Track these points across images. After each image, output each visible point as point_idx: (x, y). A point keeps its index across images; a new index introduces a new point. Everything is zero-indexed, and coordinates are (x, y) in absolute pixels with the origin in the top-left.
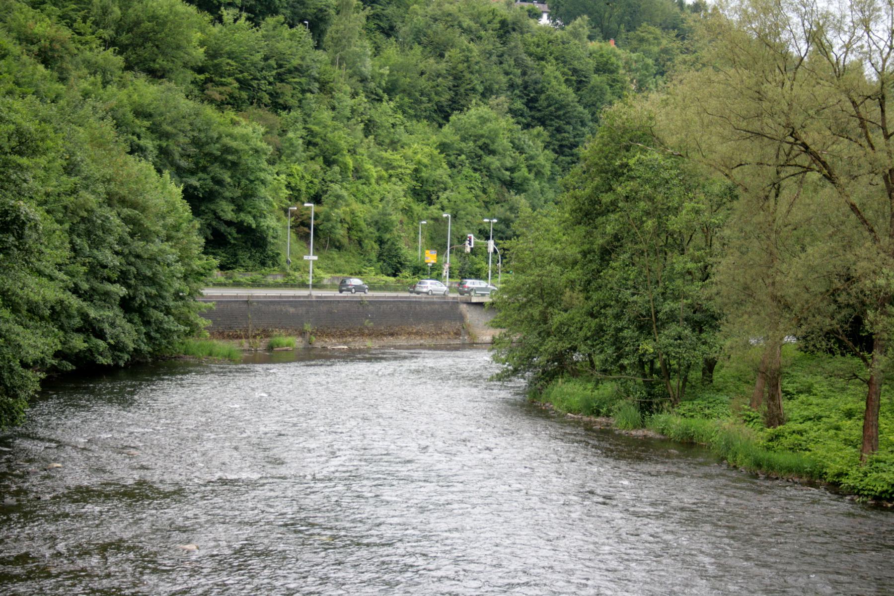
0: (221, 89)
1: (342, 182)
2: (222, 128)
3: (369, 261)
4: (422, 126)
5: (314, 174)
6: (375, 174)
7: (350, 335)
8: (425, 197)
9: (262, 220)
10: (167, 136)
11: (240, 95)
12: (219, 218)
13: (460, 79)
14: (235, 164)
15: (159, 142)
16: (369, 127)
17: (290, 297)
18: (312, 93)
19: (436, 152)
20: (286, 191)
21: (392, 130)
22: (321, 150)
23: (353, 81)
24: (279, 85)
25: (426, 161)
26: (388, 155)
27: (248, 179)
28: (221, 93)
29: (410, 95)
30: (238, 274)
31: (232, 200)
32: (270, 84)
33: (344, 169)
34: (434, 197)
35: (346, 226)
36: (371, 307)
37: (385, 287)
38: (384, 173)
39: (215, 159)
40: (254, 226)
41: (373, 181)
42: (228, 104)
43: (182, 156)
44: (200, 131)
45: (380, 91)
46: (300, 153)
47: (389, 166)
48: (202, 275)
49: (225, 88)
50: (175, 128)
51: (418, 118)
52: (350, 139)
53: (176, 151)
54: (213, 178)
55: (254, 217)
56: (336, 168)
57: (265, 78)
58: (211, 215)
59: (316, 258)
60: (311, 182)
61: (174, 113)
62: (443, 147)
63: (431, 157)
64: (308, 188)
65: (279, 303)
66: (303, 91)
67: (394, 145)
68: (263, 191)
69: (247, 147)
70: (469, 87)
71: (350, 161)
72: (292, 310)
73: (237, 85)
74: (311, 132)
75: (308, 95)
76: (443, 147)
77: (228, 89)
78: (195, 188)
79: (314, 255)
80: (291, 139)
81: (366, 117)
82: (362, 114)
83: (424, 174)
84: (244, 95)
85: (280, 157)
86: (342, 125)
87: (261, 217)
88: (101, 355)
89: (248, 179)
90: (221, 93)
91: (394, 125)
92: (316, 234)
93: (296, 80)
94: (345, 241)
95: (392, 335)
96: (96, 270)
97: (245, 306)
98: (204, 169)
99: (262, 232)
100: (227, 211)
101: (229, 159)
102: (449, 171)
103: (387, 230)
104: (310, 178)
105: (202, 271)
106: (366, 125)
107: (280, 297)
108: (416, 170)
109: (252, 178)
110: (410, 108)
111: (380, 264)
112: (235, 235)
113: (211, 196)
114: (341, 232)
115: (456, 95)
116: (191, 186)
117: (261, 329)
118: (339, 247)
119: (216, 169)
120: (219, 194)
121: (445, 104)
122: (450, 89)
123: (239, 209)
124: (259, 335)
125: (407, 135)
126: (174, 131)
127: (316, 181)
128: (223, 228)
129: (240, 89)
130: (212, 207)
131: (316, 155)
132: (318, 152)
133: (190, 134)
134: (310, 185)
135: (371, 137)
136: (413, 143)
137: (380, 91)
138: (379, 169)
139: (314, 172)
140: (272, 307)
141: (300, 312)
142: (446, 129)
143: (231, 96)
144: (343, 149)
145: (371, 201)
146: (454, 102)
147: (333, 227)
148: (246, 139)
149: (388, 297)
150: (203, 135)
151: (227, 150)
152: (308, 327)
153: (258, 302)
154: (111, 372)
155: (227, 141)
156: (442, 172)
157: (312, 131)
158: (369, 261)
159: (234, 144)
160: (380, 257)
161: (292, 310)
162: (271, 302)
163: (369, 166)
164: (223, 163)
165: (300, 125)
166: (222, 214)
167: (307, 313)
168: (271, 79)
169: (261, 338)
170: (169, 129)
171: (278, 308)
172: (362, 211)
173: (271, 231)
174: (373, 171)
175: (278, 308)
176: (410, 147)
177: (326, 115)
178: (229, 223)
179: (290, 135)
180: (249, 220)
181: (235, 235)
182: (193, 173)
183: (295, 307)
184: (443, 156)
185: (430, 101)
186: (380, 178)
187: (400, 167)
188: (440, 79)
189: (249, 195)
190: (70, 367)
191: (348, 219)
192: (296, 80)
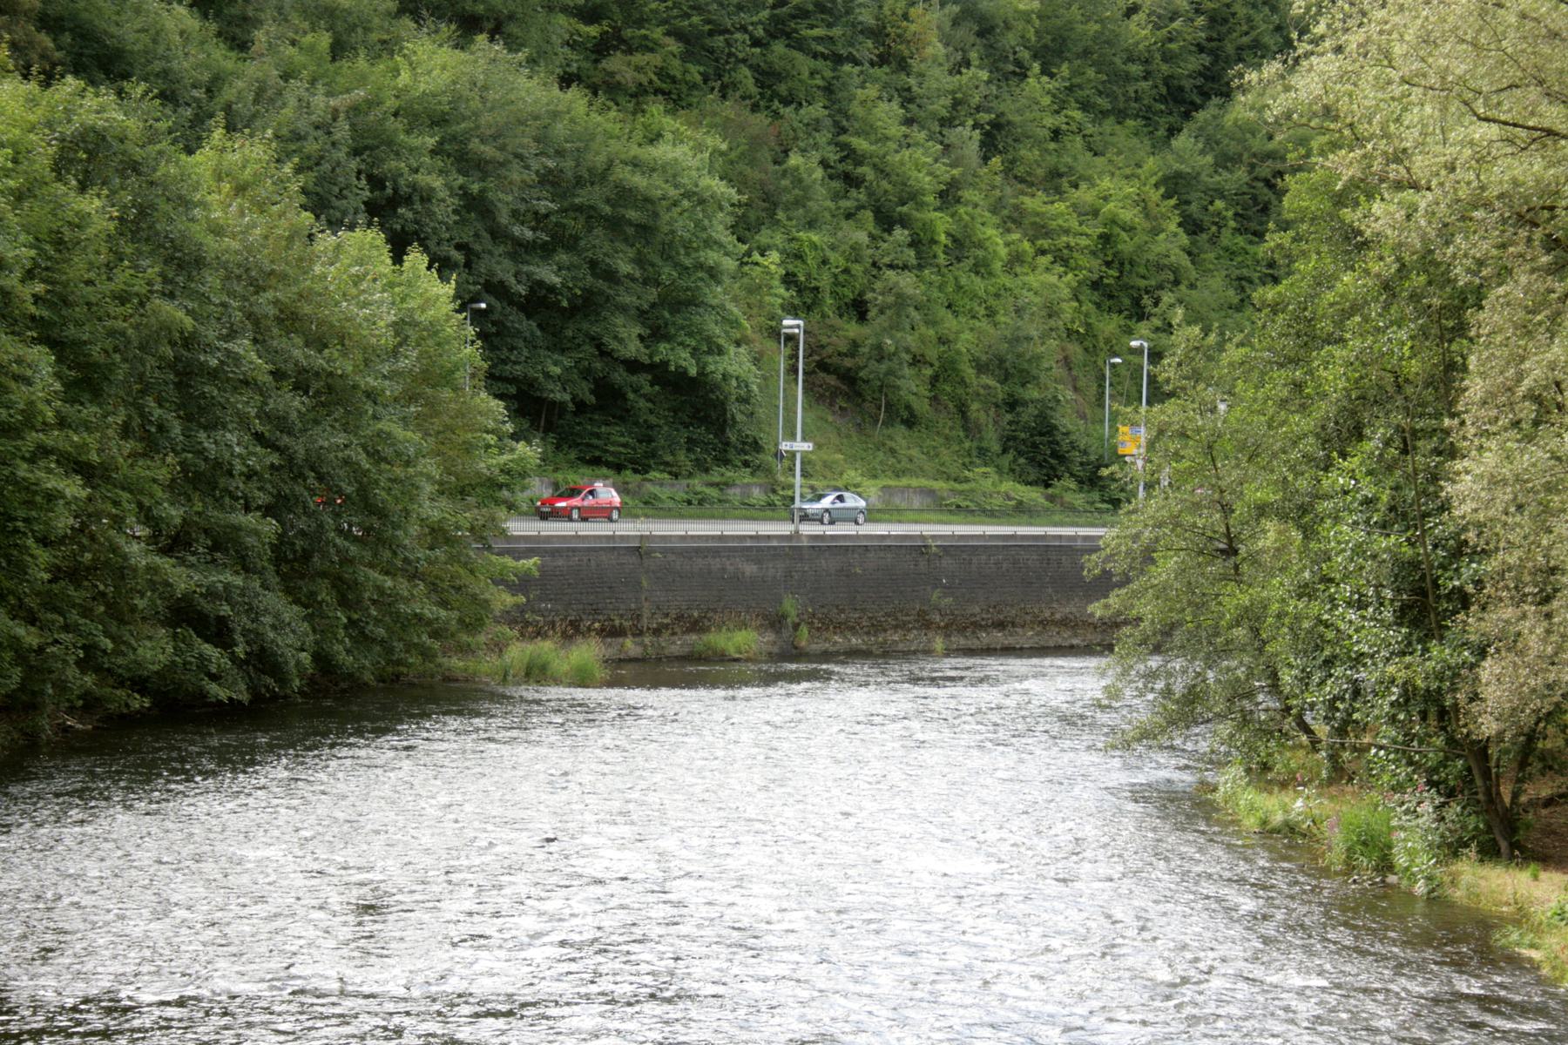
0: (638, 59)
1: (920, 267)
2: (615, 147)
3: (982, 452)
4: (1123, 136)
5: (855, 254)
6: (1003, 252)
7: (896, 627)
8: (1127, 302)
9: (710, 359)
10: (481, 167)
11: (686, 71)
12: (604, 353)
13: (1226, 21)
14: (645, 231)
15: (461, 180)
16: (994, 137)
17: (744, 537)
18: (857, 63)
19: (1155, 196)
20: (782, 291)
21: (1052, 145)
22: (870, 194)
23: (960, 33)
24: (779, 47)
25: (1128, 215)
26: (1034, 202)
27: (677, 265)
28: (638, 69)
29: (1098, 66)
30: (658, 484)
31: (642, 315)
32: (756, 43)
33: (920, 242)
34: (1147, 301)
35: (928, 372)
36: (947, 562)
37: (1021, 511)
38: (1026, 245)
39: (589, 213)
40: (693, 372)
41: (997, 266)
42: (657, 91)
43: (515, 214)
44: (560, 153)
45: (1025, 55)
46: (821, 198)
47: (1040, 230)
48: (500, 486)
49: (648, 57)
50: (502, 148)
51: (1121, 115)
52: (940, 168)
53: (504, 202)
54: (593, 264)
55: (695, 352)
56: (900, 234)
57: (743, 29)
58: (589, 349)
59: (807, 446)
60: (846, 271)
61: (500, 117)
62: (1174, 185)
63: (1142, 203)
64: (836, 283)
65: (716, 552)
66: (838, 60)
67: (1055, 181)
68: (717, 294)
69: (673, 193)
70: (1245, 40)
71: (942, 224)
72: (750, 569)
73: (673, 46)
74: (850, 154)
75: (847, 68)
76: (1174, 185)
77: (655, 59)
78: (552, 289)
79: (804, 439)
80: (797, 169)
81: (985, 117)
82: (978, 109)
83: (1126, 245)
84: (695, 72)
85: (772, 214)
86: (923, 135)
87: (710, 352)
88: (214, 678)
89: (677, 265)
90: (638, 69)
91: (1056, 134)
92: (847, 388)
93: (817, 32)
94: (922, 406)
95: (1001, 625)
96: (202, 479)
97: (634, 559)
98: (571, 244)
99: (716, 387)
100: (629, 339)
101: (633, 219)
102: (1184, 239)
103: (1026, 378)
104: (842, 262)
105: (502, 479)
106: (987, 134)
107: (721, 538)
108: (1106, 239)
109: (687, 262)
110: (1100, 93)
111: (1010, 456)
112: (647, 389)
113: (587, 305)
114: (912, 387)
115: (1216, 58)
116: (541, 283)
117: (673, 614)
118: (911, 422)
119: (598, 242)
120: (608, 299)
121: (1187, 84)
122: (1201, 49)
123: (657, 334)
124: (667, 626)
125: (1089, 154)
126: (500, 156)
127: (857, 269)
128: (619, 376)
129: (686, 57)
130: (595, 330)
131: (860, 207)
132: (863, 197)
133: (535, 165)
134: (841, 278)
135: (996, 161)
136: (1101, 174)
137: (1025, 55)
138: (1015, 236)
139: (855, 248)
140: (700, 563)
141: (771, 572)
142: (1182, 141)
143: (662, 73)
144: (922, 192)
145: (991, 313)
146: (1213, 79)
147: (890, 372)
148: (670, 172)
149: (992, 537)
150: (568, 164)
151: (625, 195)
152: (790, 606)
153: (664, 551)
154: (228, 715)
155: (623, 174)
156: (1171, 243)
157: (854, 151)
158: (982, 452)
159: (639, 181)
160: (1008, 442)
161: (750, 569)
162: (698, 550)
163: (990, 232)
164: (615, 225)
165: (823, 137)
166: (614, 345)
167: (788, 574)
168: (760, 32)
169: (667, 632)
170: (488, 151)
171: (716, 564)
172: (968, 338)
173: (734, 383)
174: (997, 241)
175: (716, 564)
176: (1093, 185)
177: (888, 114)
178: (633, 366)
179: (795, 160)
180: (682, 359)
181: (647, 389)
182: (545, 251)
183: (758, 562)
184: (1173, 202)
185: (1147, 76)
186: (1016, 259)
187: (1067, 232)
188: (1177, 24)
189: (684, 302)
190: (139, 702)
191: (932, 353)
192: (817, 32)
